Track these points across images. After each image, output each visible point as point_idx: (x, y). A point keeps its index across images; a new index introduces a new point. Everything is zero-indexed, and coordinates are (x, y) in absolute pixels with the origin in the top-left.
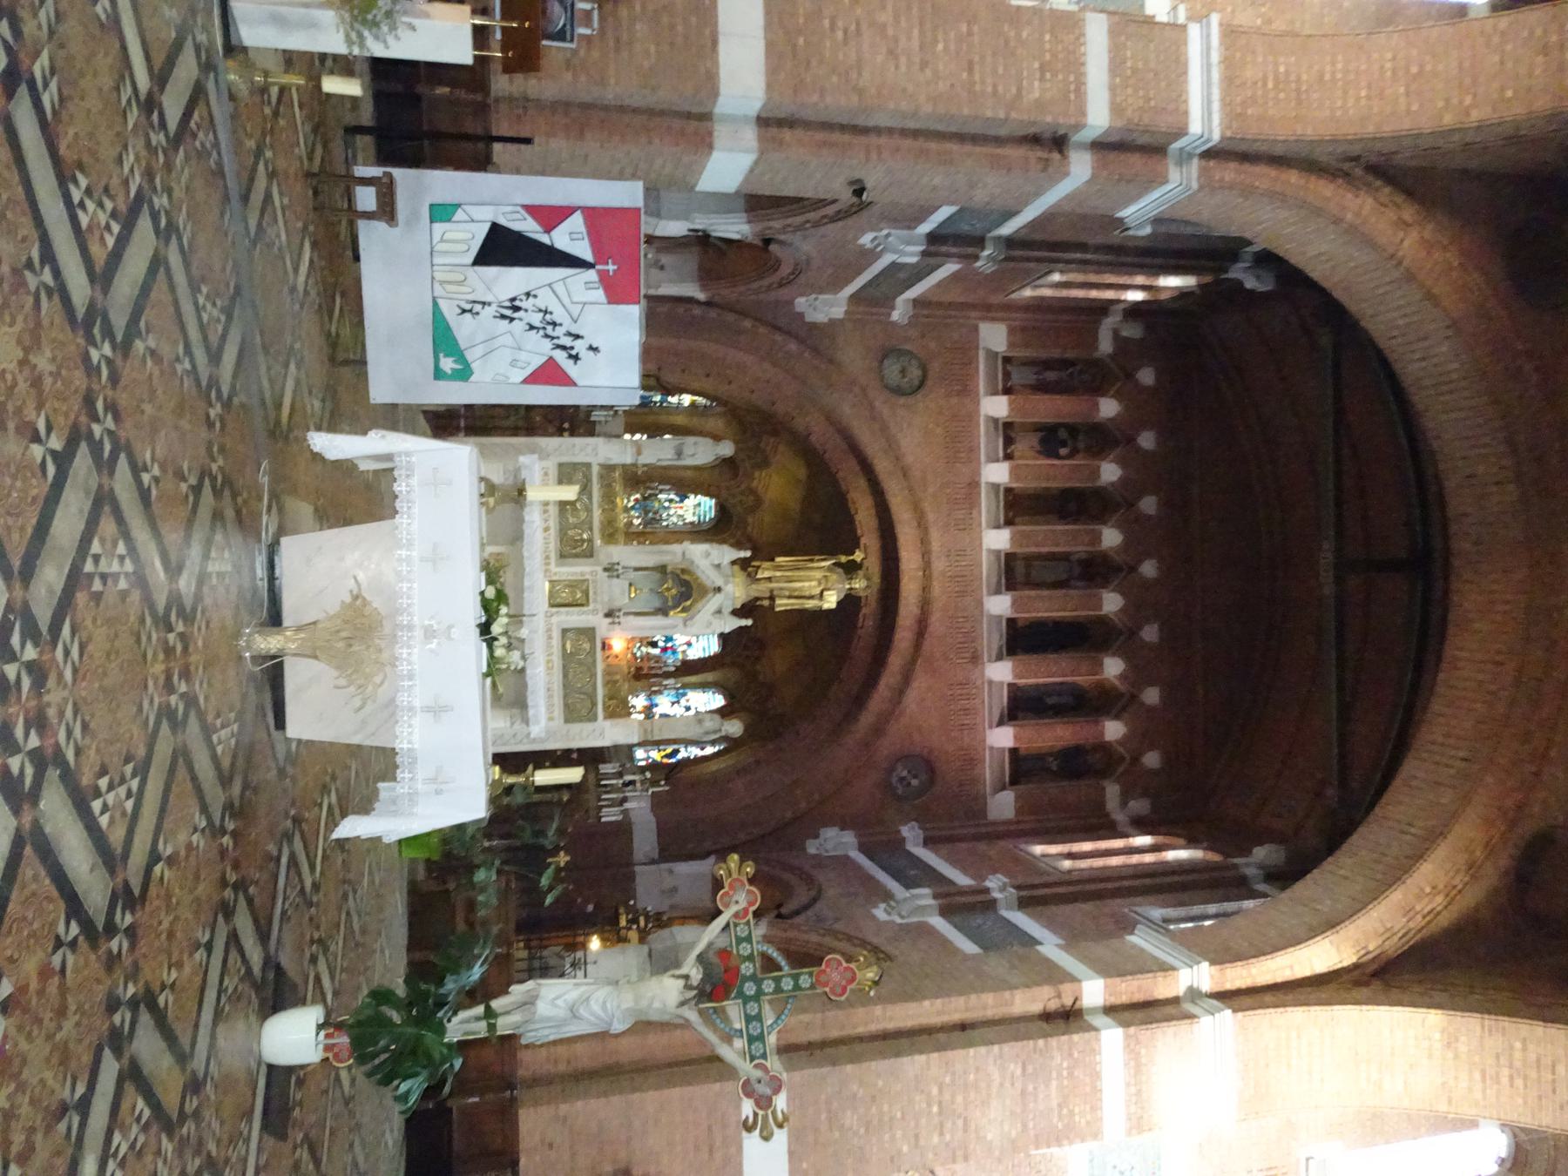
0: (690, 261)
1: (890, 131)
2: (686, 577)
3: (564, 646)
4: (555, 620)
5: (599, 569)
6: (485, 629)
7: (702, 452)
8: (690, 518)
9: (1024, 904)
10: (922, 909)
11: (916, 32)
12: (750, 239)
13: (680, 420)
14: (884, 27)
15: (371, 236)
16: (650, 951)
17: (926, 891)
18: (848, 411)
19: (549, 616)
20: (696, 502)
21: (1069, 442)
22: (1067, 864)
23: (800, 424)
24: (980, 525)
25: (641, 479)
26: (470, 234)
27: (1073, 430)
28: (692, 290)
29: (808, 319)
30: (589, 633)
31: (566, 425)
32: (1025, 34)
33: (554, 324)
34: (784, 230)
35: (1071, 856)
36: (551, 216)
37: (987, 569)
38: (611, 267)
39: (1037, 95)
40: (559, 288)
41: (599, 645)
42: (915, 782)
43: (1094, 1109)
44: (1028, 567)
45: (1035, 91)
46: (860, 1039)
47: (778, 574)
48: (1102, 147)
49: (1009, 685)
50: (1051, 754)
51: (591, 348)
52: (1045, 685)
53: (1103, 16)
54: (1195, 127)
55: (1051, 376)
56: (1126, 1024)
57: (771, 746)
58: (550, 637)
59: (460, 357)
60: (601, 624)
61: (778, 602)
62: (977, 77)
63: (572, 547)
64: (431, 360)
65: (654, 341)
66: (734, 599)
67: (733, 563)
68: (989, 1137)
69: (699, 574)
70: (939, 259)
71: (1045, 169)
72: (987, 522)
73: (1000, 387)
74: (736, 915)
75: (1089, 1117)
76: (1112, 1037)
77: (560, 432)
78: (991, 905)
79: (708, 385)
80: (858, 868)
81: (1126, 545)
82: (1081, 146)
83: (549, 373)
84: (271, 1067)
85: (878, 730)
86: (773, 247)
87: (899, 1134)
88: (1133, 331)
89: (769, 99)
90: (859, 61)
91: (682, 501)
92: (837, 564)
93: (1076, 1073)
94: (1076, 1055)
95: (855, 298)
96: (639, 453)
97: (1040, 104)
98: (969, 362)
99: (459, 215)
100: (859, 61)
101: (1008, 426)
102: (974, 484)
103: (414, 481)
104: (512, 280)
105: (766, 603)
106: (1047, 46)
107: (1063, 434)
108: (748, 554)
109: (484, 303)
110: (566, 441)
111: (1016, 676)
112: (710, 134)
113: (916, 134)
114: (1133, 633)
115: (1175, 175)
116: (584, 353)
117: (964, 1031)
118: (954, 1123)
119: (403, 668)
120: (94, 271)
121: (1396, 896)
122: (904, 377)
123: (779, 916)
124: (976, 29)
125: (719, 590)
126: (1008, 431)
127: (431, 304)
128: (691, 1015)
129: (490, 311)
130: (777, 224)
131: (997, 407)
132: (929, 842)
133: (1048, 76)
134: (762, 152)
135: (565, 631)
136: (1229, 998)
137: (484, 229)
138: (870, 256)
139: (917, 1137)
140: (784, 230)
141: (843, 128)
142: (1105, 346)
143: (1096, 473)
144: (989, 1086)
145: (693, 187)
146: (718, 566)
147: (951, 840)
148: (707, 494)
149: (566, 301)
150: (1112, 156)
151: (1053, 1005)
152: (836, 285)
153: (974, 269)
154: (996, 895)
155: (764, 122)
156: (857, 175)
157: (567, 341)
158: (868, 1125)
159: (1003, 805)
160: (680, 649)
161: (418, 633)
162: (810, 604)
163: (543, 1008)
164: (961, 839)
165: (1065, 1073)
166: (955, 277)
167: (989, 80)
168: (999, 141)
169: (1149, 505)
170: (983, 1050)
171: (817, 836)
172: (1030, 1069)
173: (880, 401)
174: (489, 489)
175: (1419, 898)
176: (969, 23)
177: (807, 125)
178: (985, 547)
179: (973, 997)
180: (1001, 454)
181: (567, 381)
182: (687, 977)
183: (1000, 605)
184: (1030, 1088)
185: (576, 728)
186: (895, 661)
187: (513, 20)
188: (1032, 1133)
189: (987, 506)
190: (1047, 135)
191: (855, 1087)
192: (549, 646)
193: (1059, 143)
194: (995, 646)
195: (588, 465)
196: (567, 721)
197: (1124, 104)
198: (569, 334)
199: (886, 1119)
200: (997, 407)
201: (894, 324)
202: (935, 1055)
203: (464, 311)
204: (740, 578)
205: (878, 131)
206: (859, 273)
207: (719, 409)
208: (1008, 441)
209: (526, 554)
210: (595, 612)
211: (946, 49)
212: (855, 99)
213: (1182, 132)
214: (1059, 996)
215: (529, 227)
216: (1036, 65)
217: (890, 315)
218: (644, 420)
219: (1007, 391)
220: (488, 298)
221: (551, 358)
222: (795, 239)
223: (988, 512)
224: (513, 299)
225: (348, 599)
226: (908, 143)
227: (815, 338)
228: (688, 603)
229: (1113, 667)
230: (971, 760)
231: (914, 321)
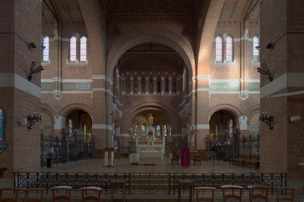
9: (188, 94)
27: (134, 83)
28: (119, 128)
37: (150, 95)
48: (106, 89)
54: (103, 78)
60: (154, 141)
88: (122, 75)
101: (134, 92)
102: (140, 96)
114: (159, 76)
115: (108, 80)
120: (233, 121)
121: (187, 54)
126: (135, 91)
131: (132, 93)
136: (196, 75)
138: (116, 110)
159: (178, 93)
169: (143, 73)
183: (155, 93)
186: (150, 108)
193: (106, 93)
213: (104, 79)
227: (124, 116)
229: (163, 79)
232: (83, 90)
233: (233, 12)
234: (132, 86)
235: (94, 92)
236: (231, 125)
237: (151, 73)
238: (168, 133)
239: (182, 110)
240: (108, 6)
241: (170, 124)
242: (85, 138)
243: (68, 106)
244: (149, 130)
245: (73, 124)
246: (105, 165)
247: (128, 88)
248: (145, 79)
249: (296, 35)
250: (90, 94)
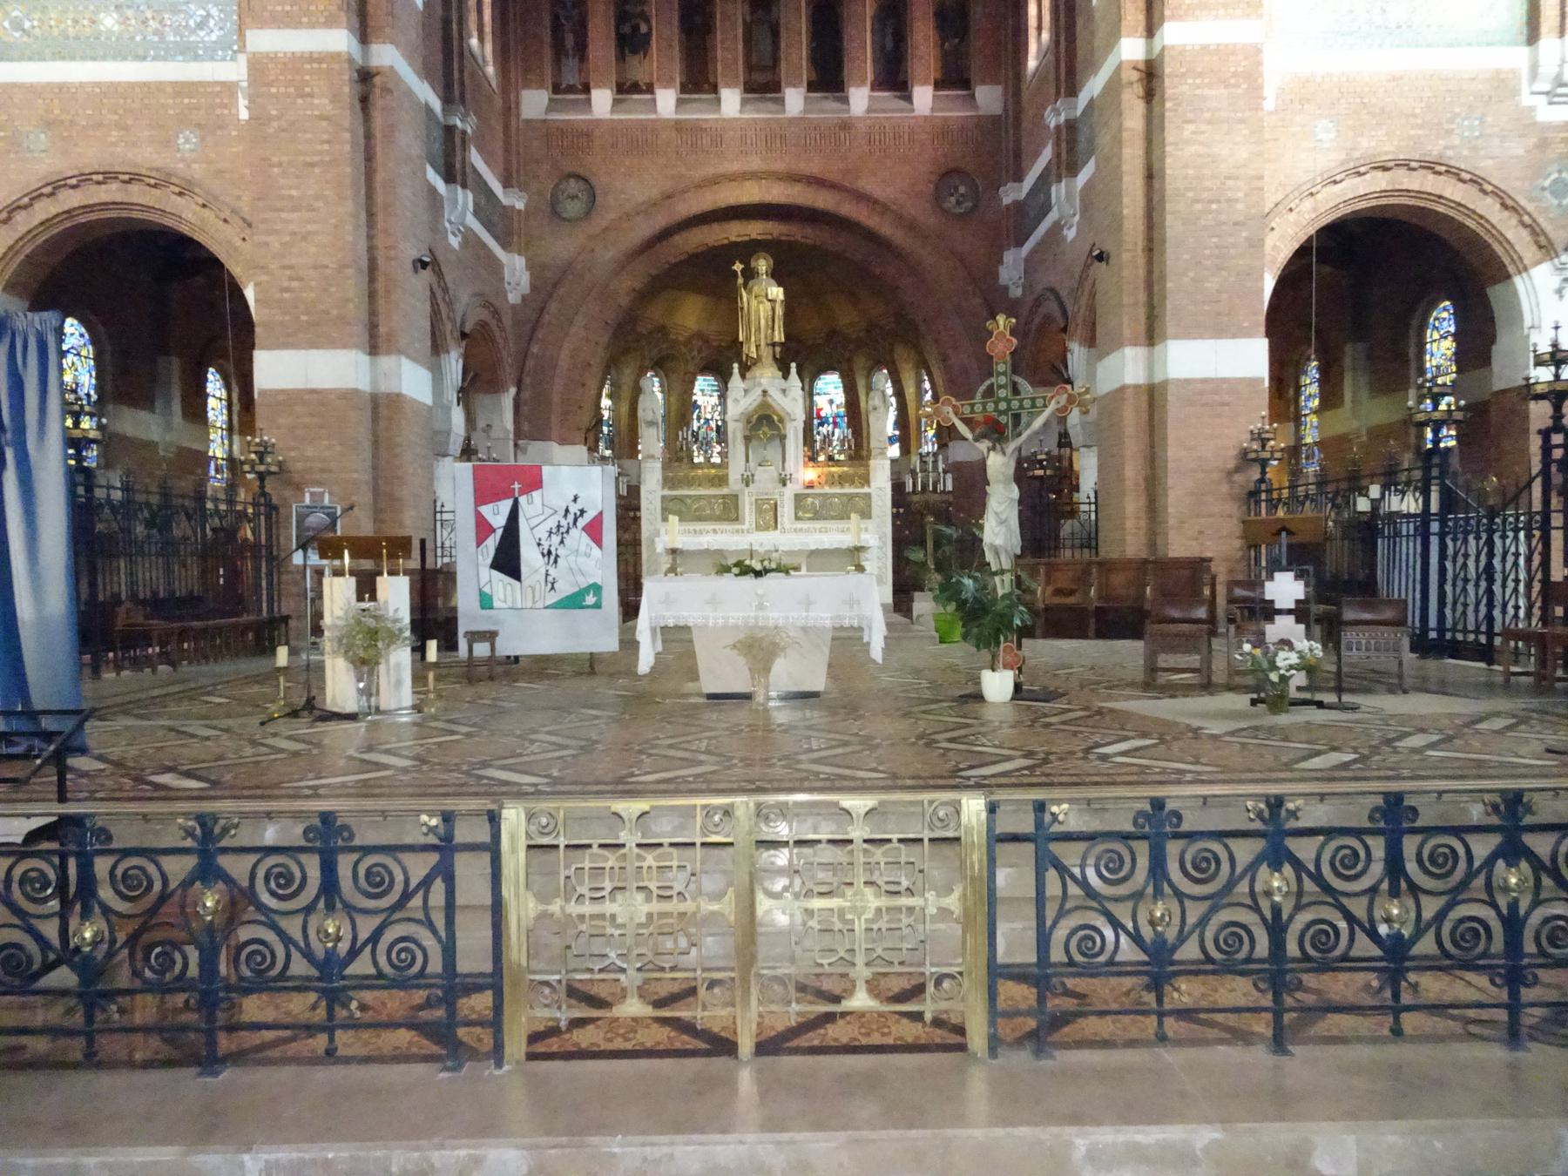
0: (482, 400)
1: (370, 237)
2: (754, 419)
3: (809, 519)
4: (787, 526)
5: (747, 490)
6: (758, 574)
7: (654, 390)
9: (1073, 92)
10: (1069, 195)
11: (284, 215)
12: (462, 350)
13: (624, 409)
14: (285, 244)
15: (506, 647)
16: (1084, 446)
17: (1053, 189)
18: (608, 254)
19: (784, 531)
20: (700, 393)
21: (633, 22)
22: (1046, 36)
23: (624, 301)
24: (716, 120)
25: (677, 456)
26: (499, 584)
28: (508, 399)
29: (527, 291)
30: (799, 498)
31: (632, 514)
32: (274, 113)
33: (559, 526)
34: (453, 321)
35: (1039, 28)
36: (483, 529)
37: (760, 113)
38: (517, 486)
39: (325, 101)
40: (534, 522)
41: (810, 491)
42: (962, 190)
43: (1234, 53)
45: (323, 103)
46: (1150, 272)
47: (753, 339)
48: (364, 36)
49: (873, 89)
50: (942, 45)
51: (575, 500)
52: (874, 52)
53: (249, 34)
55: (570, 40)
56: (1162, 20)
57: (923, 328)
58: (801, 530)
59: (586, 590)
61: (777, 339)
62: (317, 159)
63: (729, 511)
64: (589, 610)
65: (554, 433)
66: (774, 377)
67: (743, 376)
68: (1245, 155)
69: (751, 408)
70: (468, 170)
71: (389, 91)
72: (710, 112)
73: (583, 97)
74: (956, 414)
75: (1241, 57)
76: (1172, 34)
77: (637, 520)
78: (1071, 126)
79: (592, 384)
80: (1034, 251)
82: (365, 54)
83: (594, 530)
84: (1012, 699)
85: (911, 226)
86: (467, 330)
87: (1231, 240)
89: (356, 346)
90: (315, 267)
91: (699, 407)
92: (745, 285)
93: (1199, 70)
94: (1183, 70)
95: (506, 245)
96: (652, 457)
97: (335, 98)
98: (564, 131)
99: (487, 589)
100: (315, 267)
102: (678, 126)
103: (667, 614)
104: (529, 555)
105: (778, 349)
106: (282, 90)
107: (626, 29)
108: (736, 366)
109: (547, 575)
110: (645, 514)
111: (863, 82)
112: (388, 395)
113: (371, 215)
116: (579, 505)
117: (1152, 175)
118: (1230, 189)
119: (781, 622)
120: (1460, 316)
122: (577, 197)
123: (1064, 330)
124: (275, 160)
125: (765, 392)
126: (626, 88)
127: (548, 611)
128: (1011, 446)
129: (552, 571)
130: (449, 326)
131: (602, 100)
132: (1019, 178)
133: (307, 90)
134: (399, 352)
135: (797, 518)
137: (495, 573)
138: (469, 239)
139: (1236, 224)
140: (453, 321)
141: (372, 279)
144: (1200, 156)
145: (430, 408)
146: (746, 391)
147: (1018, 155)
148: (692, 383)
149: (542, 518)
150: (371, 23)
151: (1139, 89)
152: (495, 266)
153: (474, 132)
154: (1062, 118)
155: (374, 349)
156: (409, 266)
157: (571, 518)
159: (988, 98)
160: (835, 410)
161: (761, 614)
162: (779, 311)
163: (999, 542)
164: (1018, 141)
165: (1198, 81)
166: (480, 150)
167: (319, 147)
168: (368, 136)
170: (1168, 161)
171: (1006, 288)
172: (1190, 116)
173: (602, 220)
174: (672, 570)
176: (272, 166)
177: (373, 313)
178: (738, 115)
179: (1125, 167)
180: (648, 96)
181: (600, 516)
182: (989, 450)
183: (795, 99)
184: (1207, 115)
185: (875, 510)
186: (847, 209)
187: (381, 553)
188: (1248, 114)
190: (358, 87)
191: (1186, 279)
192: (808, 531)
193: (365, 76)
194: (836, 105)
195: (664, 498)
196: (870, 518)
197: (326, 14)
198: (565, 516)
199: (1217, 252)
200: (602, 100)
201: (527, 206)
202: (1168, 206)
203: (553, 588)
204: (756, 372)
205: (371, 249)
206: (484, 245)
207: (613, 371)
208: (635, 88)
209: (734, 548)
210: (782, 495)
211: (297, 188)
212: (350, 272)
214: (1131, 84)
215: (492, 543)
216: (300, 101)
217: (520, 211)
218: (626, 446)
219: (586, 89)
220: (543, 571)
221: (583, 529)
222: (460, 308)
223: (701, 111)
224: (543, 555)
225: (736, 652)
226: (380, 218)
227: (547, 284)
228: (775, 418)
230: (941, 131)
231: (523, 187)
232: (165, 53)
233: (628, 508)
235: (259, 67)
236: (1440, 349)
238: (906, 433)
241: (923, 364)
242: (217, 481)
243: (36, 196)
245: (98, 358)
250: (229, 88)
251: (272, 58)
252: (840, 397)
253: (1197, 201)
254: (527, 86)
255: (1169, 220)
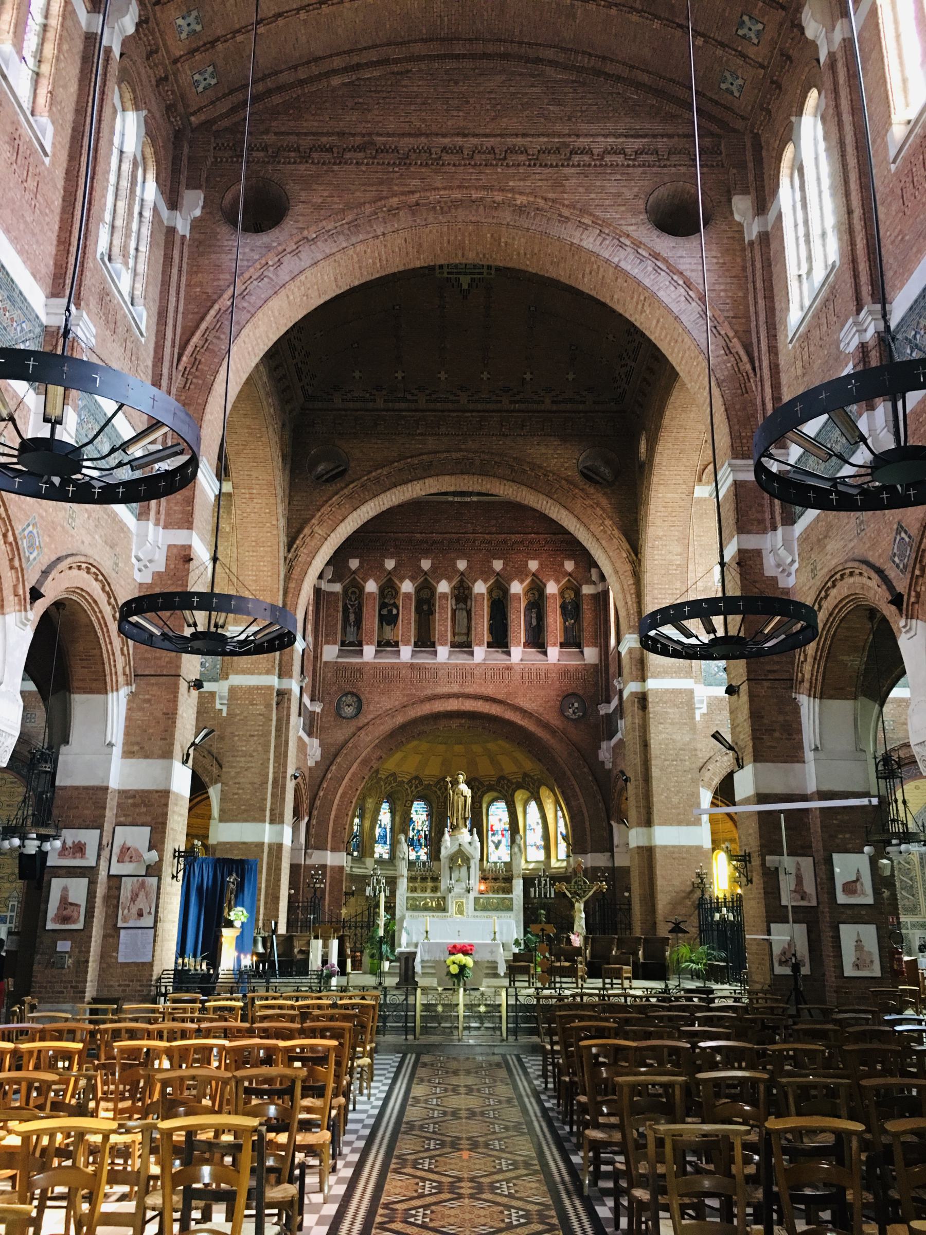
8: (424, 817)
14: (238, 773)
27: (382, 606)
42: (576, 705)
44: (459, 634)
55: (352, 617)
76: (652, 684)
81: (449, 580)
85: (546, 726)
98: (345, 668)
102: (412, 666)
107: (385, 612)
111: (519, 645)
126: (384, 644)
142: (337, 588)
143: (407, 595)
158: (678, 792)
159: (591, 654)
169: (426, 564)
171: (603, 763)
173: (363, 720)
175: (605, 532)
185: (515, 907)
186: (509, 715)
189: (424, 659)
208: (388, 644)
219: (360, 644)
229: (516, 588)
230: (565, 672)
234: (371, 621)
237: (390, 564)
239: (610, 737)
240: (517, 398)
244: (456, 848)
246: (9, 1188)
247: (351, 630)
248: (433, 590)
249: (766, 684)
251: (240, 688)
252: (505, 817)
253: (665, 760)
254: (327, 643)
255: (654, 769)
